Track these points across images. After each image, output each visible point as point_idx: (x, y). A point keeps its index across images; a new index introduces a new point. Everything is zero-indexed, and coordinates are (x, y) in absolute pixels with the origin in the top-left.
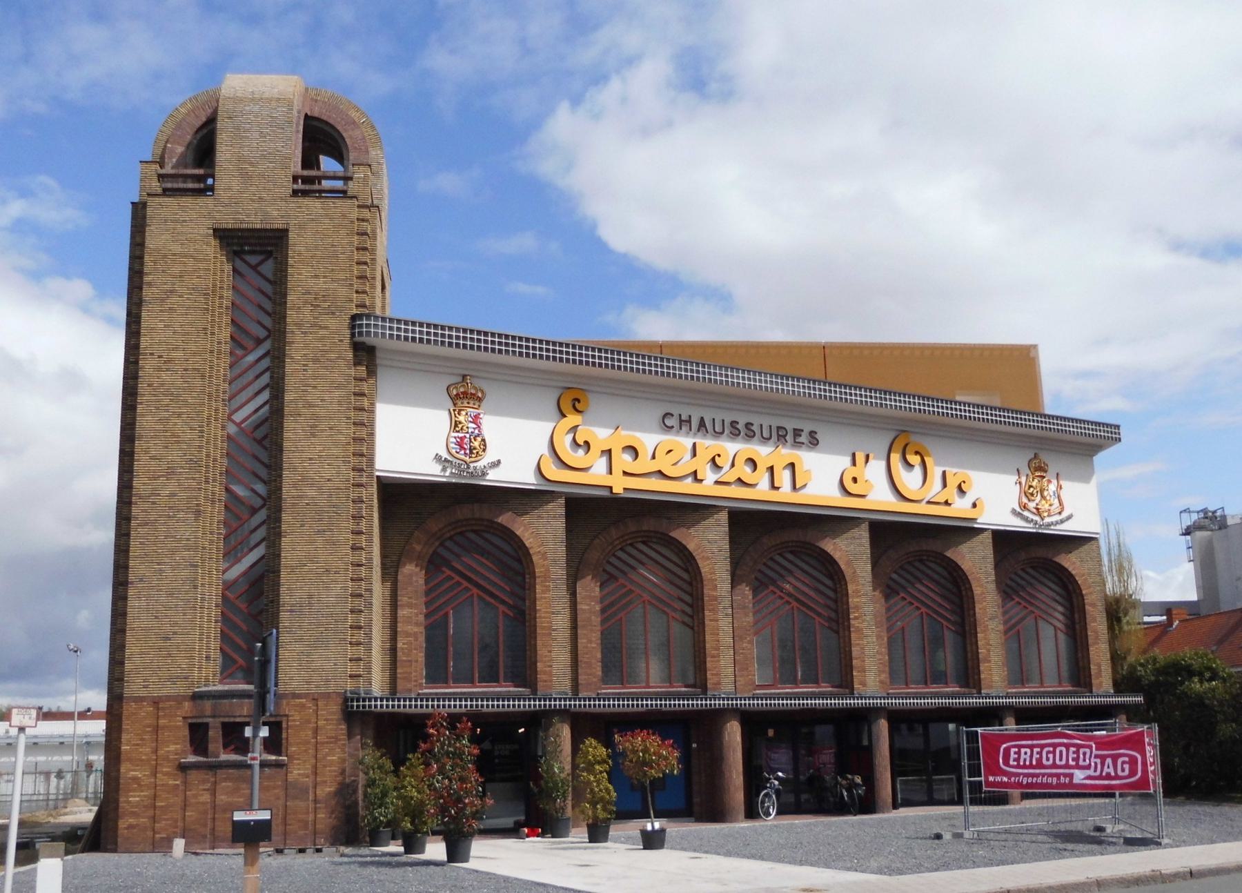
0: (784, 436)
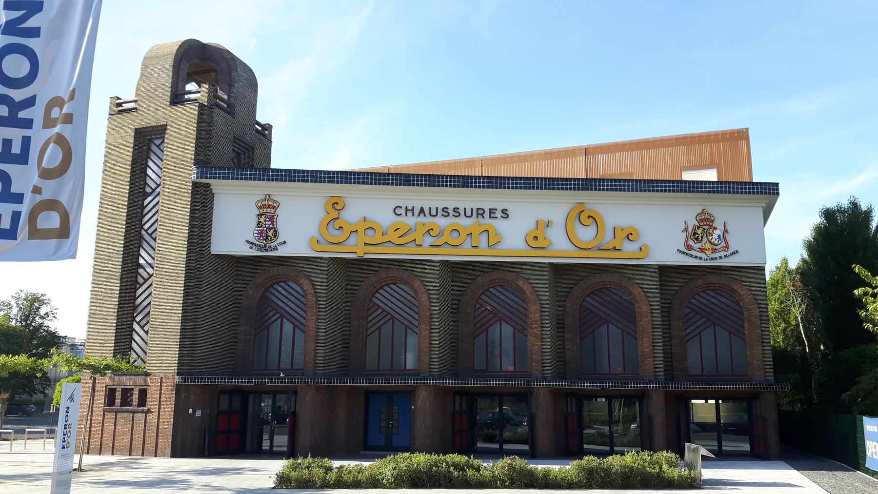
0: (482, 215)
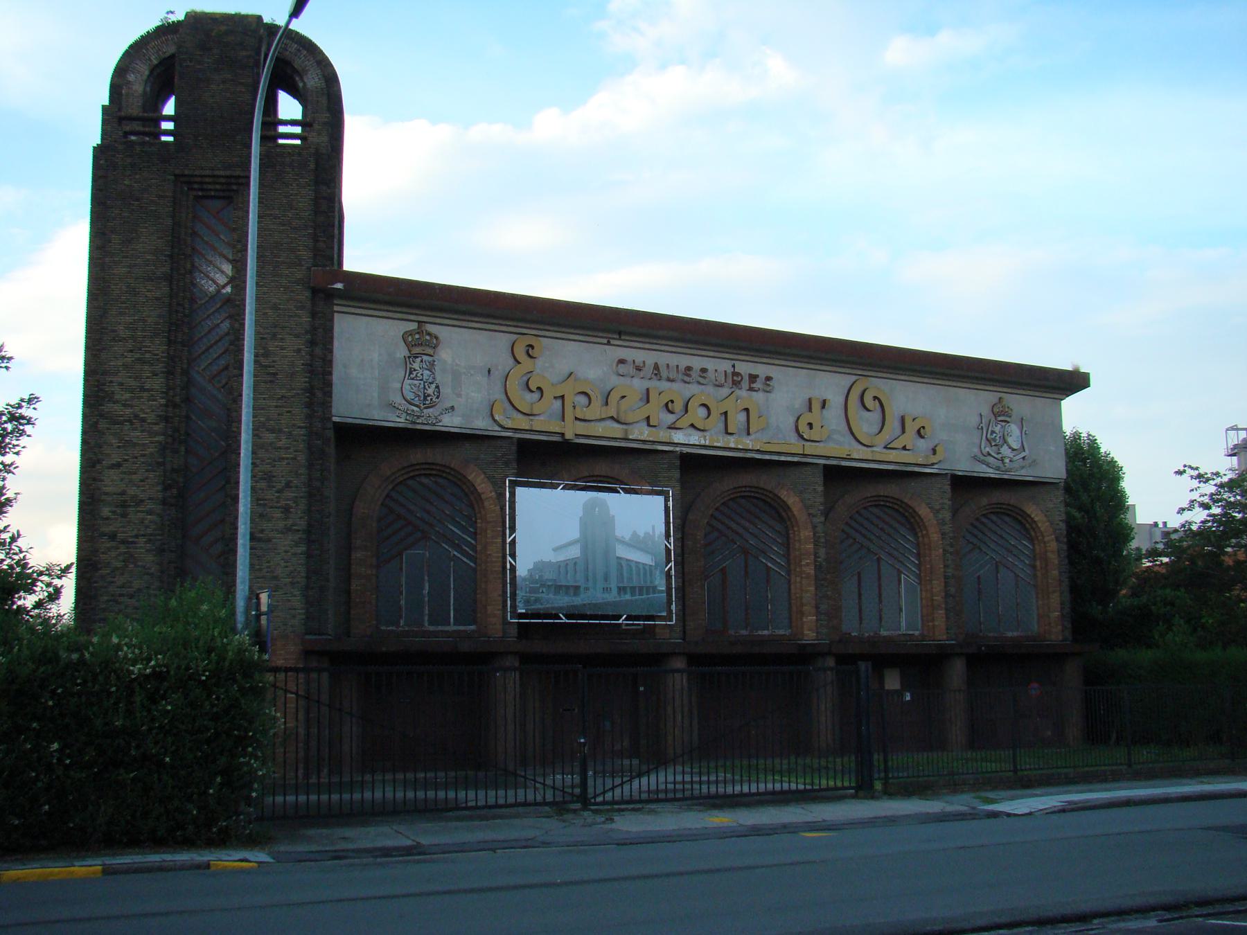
0: (739, 382)
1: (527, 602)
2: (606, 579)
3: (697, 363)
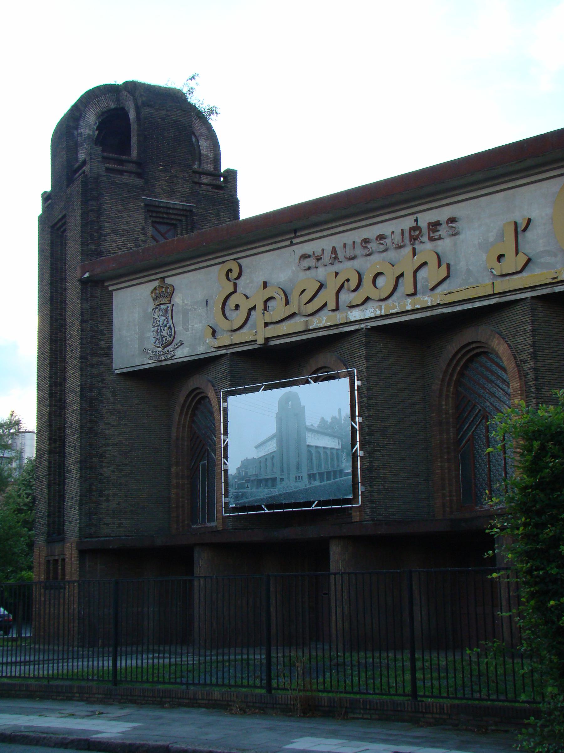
1: (237, 497)
2: (298, 468)
3: (372, 232)
